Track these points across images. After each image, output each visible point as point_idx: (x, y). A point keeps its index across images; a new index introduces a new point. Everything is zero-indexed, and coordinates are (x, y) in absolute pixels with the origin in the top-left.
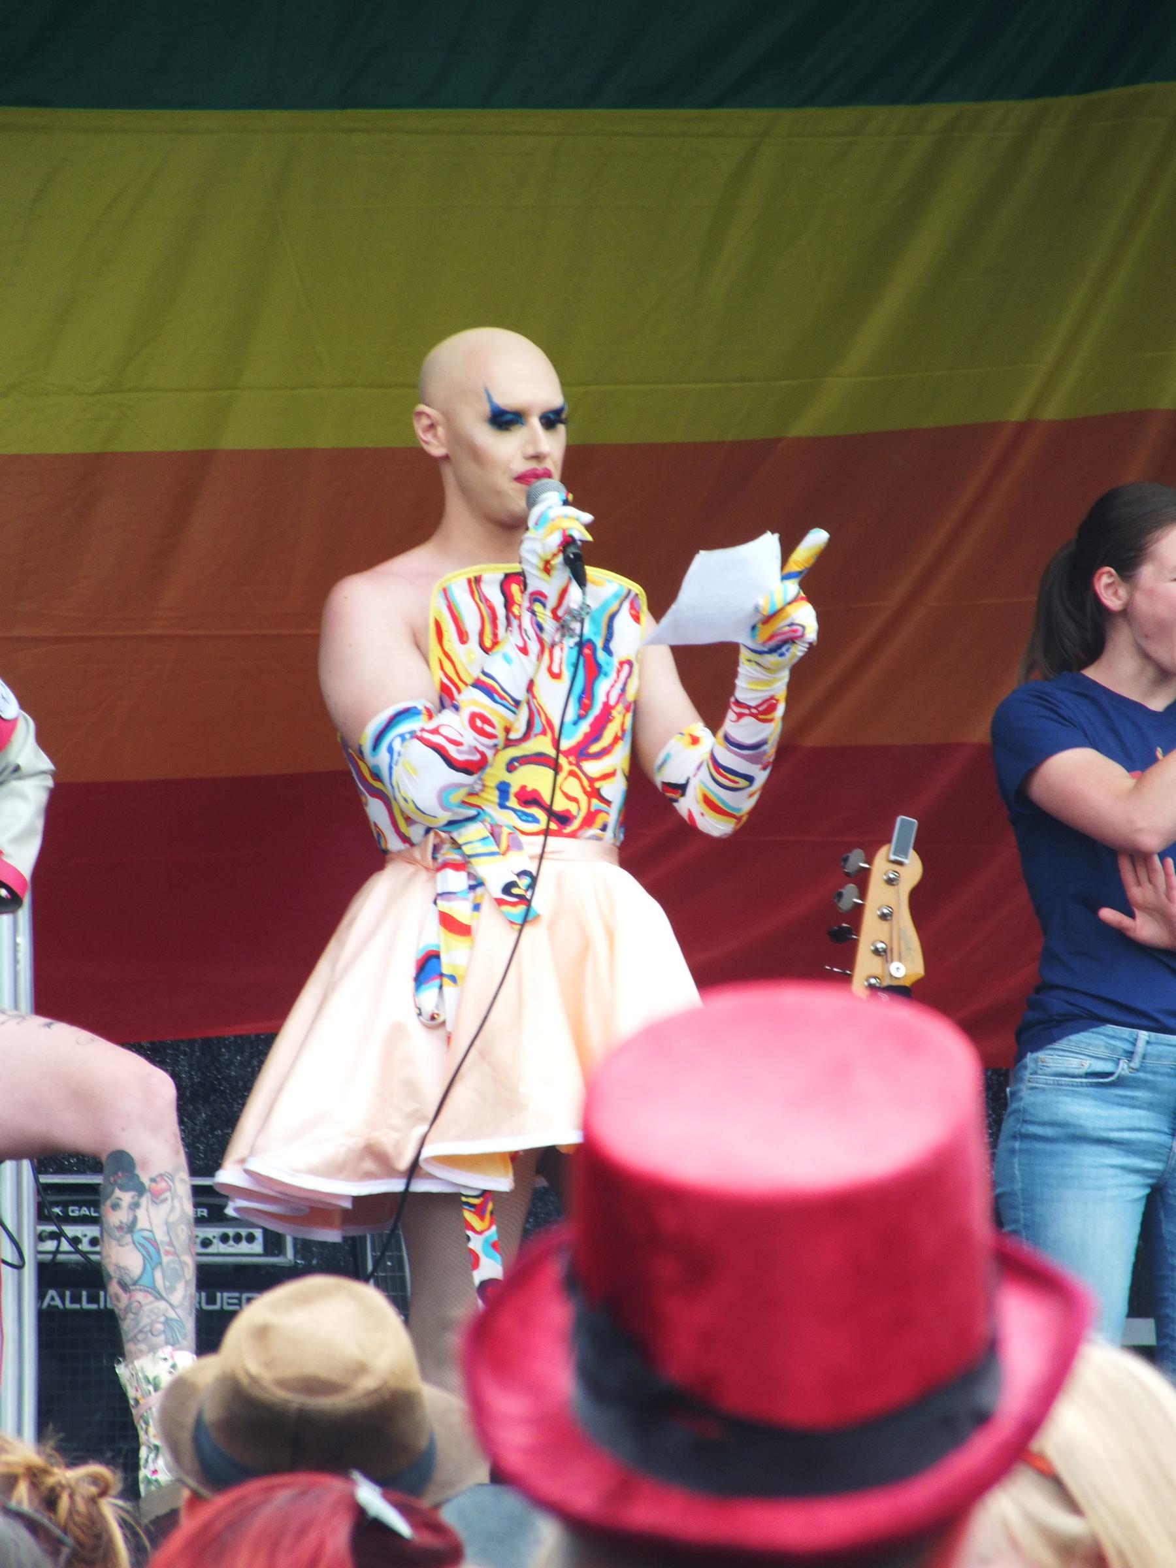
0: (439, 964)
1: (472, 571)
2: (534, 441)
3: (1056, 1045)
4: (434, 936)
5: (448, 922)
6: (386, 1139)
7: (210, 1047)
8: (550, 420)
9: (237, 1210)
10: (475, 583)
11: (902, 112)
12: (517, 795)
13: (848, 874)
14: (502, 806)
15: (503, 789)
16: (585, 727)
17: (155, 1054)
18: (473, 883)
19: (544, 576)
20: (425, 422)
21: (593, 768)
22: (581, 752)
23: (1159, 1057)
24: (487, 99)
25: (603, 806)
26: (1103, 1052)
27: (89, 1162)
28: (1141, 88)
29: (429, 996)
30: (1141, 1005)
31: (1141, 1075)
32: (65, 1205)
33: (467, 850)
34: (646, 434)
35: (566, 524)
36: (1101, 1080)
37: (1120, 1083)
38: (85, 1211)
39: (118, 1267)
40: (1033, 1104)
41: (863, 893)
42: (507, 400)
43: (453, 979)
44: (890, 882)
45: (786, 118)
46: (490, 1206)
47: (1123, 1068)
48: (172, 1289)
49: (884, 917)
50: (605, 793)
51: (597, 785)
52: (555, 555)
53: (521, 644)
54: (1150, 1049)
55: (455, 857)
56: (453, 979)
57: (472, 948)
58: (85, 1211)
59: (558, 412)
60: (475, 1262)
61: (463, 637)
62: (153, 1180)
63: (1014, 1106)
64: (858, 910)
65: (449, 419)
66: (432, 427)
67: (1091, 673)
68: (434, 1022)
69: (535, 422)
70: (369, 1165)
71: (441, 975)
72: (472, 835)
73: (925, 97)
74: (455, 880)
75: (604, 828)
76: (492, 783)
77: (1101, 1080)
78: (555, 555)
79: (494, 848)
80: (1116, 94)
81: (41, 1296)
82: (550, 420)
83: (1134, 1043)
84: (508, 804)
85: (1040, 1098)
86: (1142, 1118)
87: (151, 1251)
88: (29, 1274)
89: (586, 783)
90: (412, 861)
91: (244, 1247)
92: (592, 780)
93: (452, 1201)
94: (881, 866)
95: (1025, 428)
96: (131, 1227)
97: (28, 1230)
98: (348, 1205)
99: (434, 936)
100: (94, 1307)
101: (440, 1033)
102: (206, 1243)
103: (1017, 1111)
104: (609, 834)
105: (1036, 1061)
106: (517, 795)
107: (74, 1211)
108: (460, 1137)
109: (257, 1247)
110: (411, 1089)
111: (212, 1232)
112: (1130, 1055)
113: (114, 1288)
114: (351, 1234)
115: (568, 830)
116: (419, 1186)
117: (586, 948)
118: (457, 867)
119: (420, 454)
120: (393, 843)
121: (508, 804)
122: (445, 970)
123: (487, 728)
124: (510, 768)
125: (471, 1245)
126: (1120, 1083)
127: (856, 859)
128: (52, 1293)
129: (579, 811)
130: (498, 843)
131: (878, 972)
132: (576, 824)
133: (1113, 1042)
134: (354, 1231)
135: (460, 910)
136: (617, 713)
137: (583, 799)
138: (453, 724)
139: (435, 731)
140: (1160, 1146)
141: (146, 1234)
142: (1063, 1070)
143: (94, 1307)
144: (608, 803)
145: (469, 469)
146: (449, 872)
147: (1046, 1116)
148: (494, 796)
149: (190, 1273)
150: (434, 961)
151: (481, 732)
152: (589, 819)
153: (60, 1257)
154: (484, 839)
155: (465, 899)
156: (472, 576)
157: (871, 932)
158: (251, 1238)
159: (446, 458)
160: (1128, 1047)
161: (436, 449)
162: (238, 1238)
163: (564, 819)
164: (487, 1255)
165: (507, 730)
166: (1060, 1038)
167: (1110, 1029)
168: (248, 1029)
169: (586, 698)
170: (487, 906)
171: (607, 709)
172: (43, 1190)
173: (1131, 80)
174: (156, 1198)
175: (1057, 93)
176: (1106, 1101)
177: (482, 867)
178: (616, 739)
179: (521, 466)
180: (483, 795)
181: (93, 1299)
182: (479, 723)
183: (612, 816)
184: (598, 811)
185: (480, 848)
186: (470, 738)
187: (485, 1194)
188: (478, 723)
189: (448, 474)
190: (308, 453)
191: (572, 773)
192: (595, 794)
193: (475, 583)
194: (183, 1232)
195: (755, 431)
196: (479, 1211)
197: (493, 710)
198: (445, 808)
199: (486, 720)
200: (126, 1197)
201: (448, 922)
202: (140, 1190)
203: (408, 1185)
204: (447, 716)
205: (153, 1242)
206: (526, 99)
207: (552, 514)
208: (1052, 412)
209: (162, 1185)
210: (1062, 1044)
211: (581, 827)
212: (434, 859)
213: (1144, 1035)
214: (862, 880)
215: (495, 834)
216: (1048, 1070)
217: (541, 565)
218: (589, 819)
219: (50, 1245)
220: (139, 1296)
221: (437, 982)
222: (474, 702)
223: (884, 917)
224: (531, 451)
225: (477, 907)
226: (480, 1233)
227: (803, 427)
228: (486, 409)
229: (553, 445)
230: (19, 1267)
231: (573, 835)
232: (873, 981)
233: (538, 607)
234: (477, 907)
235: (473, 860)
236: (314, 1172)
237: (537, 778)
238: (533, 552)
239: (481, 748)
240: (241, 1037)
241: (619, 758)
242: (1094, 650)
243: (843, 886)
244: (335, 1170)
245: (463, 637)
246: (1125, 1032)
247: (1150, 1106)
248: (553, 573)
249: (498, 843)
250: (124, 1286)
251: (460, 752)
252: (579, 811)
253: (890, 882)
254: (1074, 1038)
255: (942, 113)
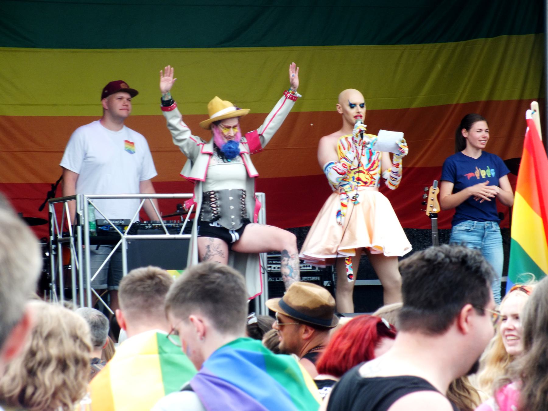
0: (341, 213)
1: (346, 136)
2: (358, 109)
3: (459, 225)
4: (340, 207)
5: (343, 205)
6: (330, 246)
7: (300, 229)
8: (362, 106)
9: (306, 262)
10: (346, 138)
11: (431, 45)
12: (356, 179)
13: (425, 192)
14: (354, 181)
15: (353, 178)
16: (370, 165)
17: (290, 230)
18: (347, 196)
19: (356, 137)
20: (338, 107)
21: (371, 173)
22: (369, 170)
23: (479, 226)
24: (351, 43)
25: (374, 180)
26: (468, 225)
27: (279, 252)
28: (476, 39)
29: (339, 219)
30: (474, 217)
31: (475, 230)
32: (272, 261)
33: (346, 190)
34: (384, 108)
35: (360, 127)
36: (468, 231)
37: (472, 231)
38: (276, 262)
39: (285, 273)
40: (455, 236)
41: (428, 195)
42: (353, 101)
43: (343, 215)
44: (433, 193)
45: (409, 46)
46: (351, 259)
47: (472, 229)
48: (295, 277)
49: (432, 200)
50: (374, 178)
51: (373, 176)
52: (358, 133)
53: (352, 150)
54: (477, 225)
55: (343, 191)
56: (343, 215)
57: (347, 209)
58: (276, 262)
59: (363, 104)
60: (347, 270)
61: (344, 149)
62: (292, 255)
63: (452, 237)
64: (427, 199)
65: (343, 106)
66: (340, 108)
67: (463, 152)
68: (340, 224)
69: (358, 106)
70: (327, 252)
71: (341, 215)
72: (347, 187)
73: (435, 42)
74: (344, 196)
75: (374, 184)
76: (351, 176)
77: (468, 231)
78: (358, 133)
79: (351, 190)
80: (471, 41)
81: (268, 279)
82: (362, 106)
83: (474, 223)
84: (354, 181)
85: (456, 235)
86: (476, 238)
87: (291, 269)
88: (266, 274)
89: (370, 176)
90: (336, 193)
91: (308, 268)
92: (371, 175)
93: (343, 259)
94: (431, 190)
95: (456, 105)
96: (287, 265)
97: (266, 265)
98: (324, 260)
99: (340, 207)
100: (278, 281)
101: (341, 226)
102: (301, 267)
103: (452, 238)
104: (376, 186)
105: (455, 228)
106: (356, 179)
107: (274, 262)
108: (345, 246)
109: (311, 268)
110: (335, 237)
111: (302, 265)
112: (473, 226)
113: (284, 277)
114: (327, 266)
115: (367, 185)
116: (339, 256)
117: (370, 208)
118: (344, 193)
119: (337, 112)
120: (334, 189)
121: (354, 181)
122: (342, 214)
123: (346, 166)
124: (355, 173)
125: (347, 267)
126: (472, 231)
127: (426, 189)
128: (270, 278)
129: (369, 181)
130: (352, 188)
131: (431, 210)
132: (368, 184)
133: (470, 224)
134: (329, 265)
135: (345, 202)
136: (376, 162)
137: (370, 179)
138: (339, 166)
139: (335, 167)
140: (480, 243)
141: (291, 266)
142: (460, 229)
143: (278, 281)
144: (375, 179)
145: (346, 115)
146: (343, 195)
147: (458, 239)
148: (352, 179)
149: (299, 274)
150: (340, 212)
151: (344, 167)
152: (371, 183)
153: (272, 271)
154: (349, 188)
155: (346, 200)
156: (346, 137)
157: (430, 203)
158: (309, 266)
159: (343, 114)
160: (472, 224)
161: (341, 112)
162: (307, 266)
163: (366, 183)
164: (350, 269)
165: (350, 167)
166: (460, 223)
167: (469, 221)
168: (305, 226)
169: (370, 159)
170: (350, 201)
171: (374, 161)
172: (268, 258)
173: (474, 38)
174: (293, 259)
175: (460, 41)
176: (469, 235)
177: (349, 194)
178: (377, 167)
179: (355, 114)
180: (350, 179)
181: (278, 279)
182: (344, 165)
183: (376, 182)
184: (373, 181)
185: (348, 190)
186: (342, 168)
187: (350, 257)
188: (344, 165)
189: (343, 117)
190: (318, 112)
191: (367, 174)
192: (372, 178)
193: (346, 138)
194: (298, 266)
195: (404, 107)
196: (348, 260)
197: (347, 163)
198: (337, 182)
199: (346, 165)
200: (286, 259)
201: (343, 205)
202: (289, 257)
203: (337, 256)
204: (338, 164)
205: (291, 267)
206: (358, 43)
207: (358, 125)
208: (462, 102)
209: (293, 256)
210: (460, 224)
211: (369, 185)
212: (340, 192)
213: (475, 222)
214: (428, 193)
215: (351, 187)
216: (458, 229)
217: (356, 135)
218: (371, 183)
219: (269, 269)
220: (289, 278)
221: (340, 216)
222: (343, 162)
223: (432, 200)
224: (357, 111)
225: (348, 201)
226: (348, 265)
227: (414, 106)
228: (348, 103)
229: (363, 111)
230: (264, 273)
231: (368, 186)
232: (430, 212)
233: (356, 143)
234: (348, 201)
235: (347, 192)
236: (315, 254)
237: (361, 176)
238: (354, 133)
239: (345, 170)
240: (307, 227)
241: (378, 171)
242: (464, 147)
243: (424, 194)
244: (319, 253)
245: (344, 149)
246: (472, 221)
247: (477, 236)
248: (358, 137)
249: (352, 188)
250: (286, 276)
251: (341, 171)
252: (369, 181)
253: (433, 193)
254: (462, 223)
255: (438, 45)
